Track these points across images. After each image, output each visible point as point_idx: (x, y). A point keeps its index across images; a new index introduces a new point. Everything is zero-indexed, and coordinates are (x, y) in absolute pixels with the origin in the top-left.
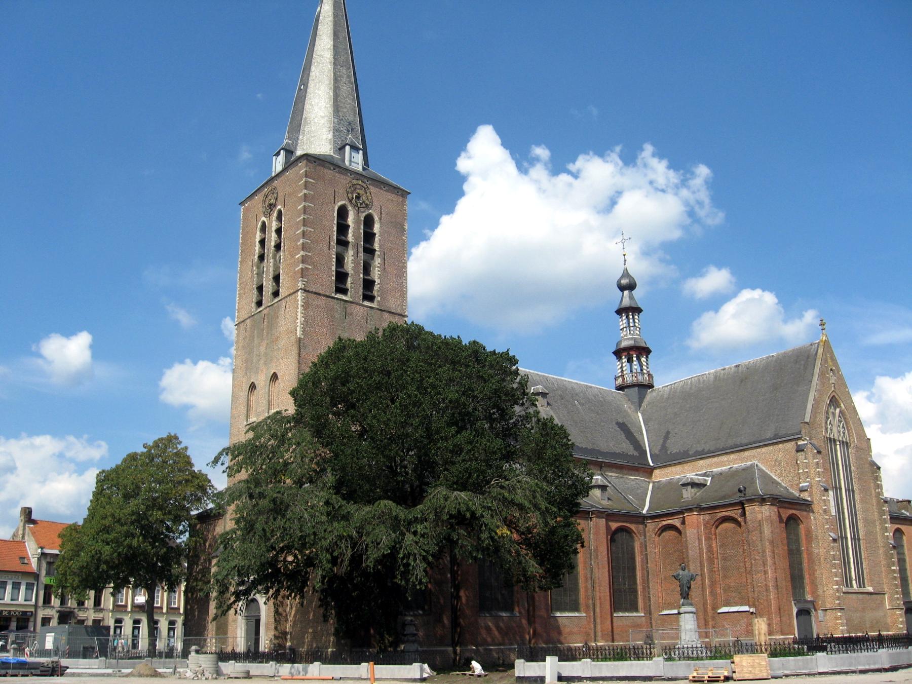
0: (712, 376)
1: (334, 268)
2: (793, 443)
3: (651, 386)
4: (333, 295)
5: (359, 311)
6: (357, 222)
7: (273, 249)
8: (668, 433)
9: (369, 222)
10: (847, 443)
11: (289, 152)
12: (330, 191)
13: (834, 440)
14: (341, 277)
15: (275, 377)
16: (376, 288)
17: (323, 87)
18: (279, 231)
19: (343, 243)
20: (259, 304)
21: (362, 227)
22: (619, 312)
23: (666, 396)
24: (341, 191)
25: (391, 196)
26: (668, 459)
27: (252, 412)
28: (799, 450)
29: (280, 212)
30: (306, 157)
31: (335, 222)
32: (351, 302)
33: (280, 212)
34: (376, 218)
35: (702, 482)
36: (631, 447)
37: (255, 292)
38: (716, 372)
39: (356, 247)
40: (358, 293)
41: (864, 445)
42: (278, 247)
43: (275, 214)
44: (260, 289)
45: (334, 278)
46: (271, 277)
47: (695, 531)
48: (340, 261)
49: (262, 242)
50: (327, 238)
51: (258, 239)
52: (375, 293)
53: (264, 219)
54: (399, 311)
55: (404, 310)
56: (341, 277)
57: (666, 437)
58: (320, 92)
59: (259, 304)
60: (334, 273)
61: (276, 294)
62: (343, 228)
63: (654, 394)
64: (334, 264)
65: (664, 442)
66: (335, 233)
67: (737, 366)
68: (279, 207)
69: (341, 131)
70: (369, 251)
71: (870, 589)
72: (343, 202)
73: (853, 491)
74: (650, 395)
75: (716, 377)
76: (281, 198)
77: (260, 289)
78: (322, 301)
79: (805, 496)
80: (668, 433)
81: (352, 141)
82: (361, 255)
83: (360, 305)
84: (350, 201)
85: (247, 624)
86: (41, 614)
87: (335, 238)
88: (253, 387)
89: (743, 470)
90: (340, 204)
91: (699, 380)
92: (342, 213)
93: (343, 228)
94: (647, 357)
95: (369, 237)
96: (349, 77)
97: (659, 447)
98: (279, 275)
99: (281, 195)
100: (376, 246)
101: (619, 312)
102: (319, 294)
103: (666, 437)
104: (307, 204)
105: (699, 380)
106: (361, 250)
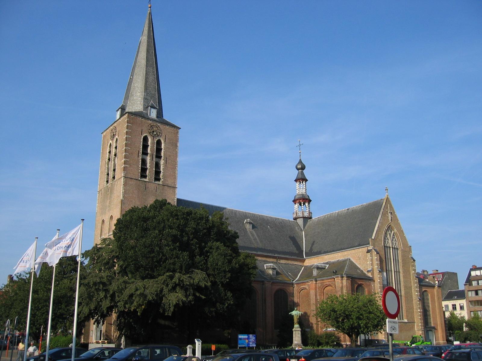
0: (336, 214)
1: (140, 166)
2: (366, 248)
3: (311, 218)
4: (139, 179)
5: (153, 185)
6: (153, 143)
7: (113, 156)
8: (314, 242)
9: (159, 143)
10: (397, 249)
11: (123, 109)
12: (140, 130)
13: (390, 247)
14: (144, 170)
15: (112, 217)
16: (161, 174)
17: (140, 78)
18: (116, 148)
19: (145, 153)
20: (107, 182)
21: (155, 146)
22: (296, 181)
23: (316, 223)
24: (145, 129)
25: (173, 129)
26: (311, 254)
27: (103, 233)
28: (368, 251)
29: (117, 139)
30: (129, 113)
31: (142, 144)
32: (148, 182)
33: (117, 139)
34: (162, 141)
35: (323, 267)
36: (295, 249)
37: (106, 176)
38: (339, 212)
39: (152, 156)
40: (152, 177)
41: (407, 249)
42: (115, 155)
43: (115, 140)
44: (108, 174)
45: (140, 171)
46: (112, 170)
47: (314, 291)
48: (144, 162)
49: (110, 152)
50: (137, 152)
51: (108, 151)
52: (161, 177)
53: (111, 142)
54: (173, 185)
55: (175, 185)
56: (144, 170)
57: (313, 244)
58: (139, 80)
59: (107, 182)
60: (140, 169)
61: (114, 178)
62: (145, 147)
63: (311, 222)
64: (140, 164)
65: (312, 246)
66: (141, 149)
67: (348, 209)
68: (117, 137)
69: (148, 99)
70: (159, 156)
71: (406, 321)
72: (146, 134)
73: (399, 272)
74: (310, 222)
75: (338, 215)
76: (117, 133)
77: (108, 174)
78: (133, 182)
79: (370, 275)
80: (314, 242)
81: (152, 104)
82: (154, 159)
83: (153, 183)
84: (150, 133)
85: (431, 321)
86: (471, 295)
87: (141, 151)
88: (103, 221)
89: (343, 261)
90: (144, 135)
91: (331, 215)
92: (145, 139)
93: (145, 147)
94: (309, 204)
95: (159, 150)
96: (153, 72)
97: (309, 249)
98: (109, 174)
99: (117, 130)
100: (162, 154)
101: (296, 181)
102: (132, 179)
103: (313, 244)
104: (128, 136)
105: (331, 215)
106: (154, 157)
